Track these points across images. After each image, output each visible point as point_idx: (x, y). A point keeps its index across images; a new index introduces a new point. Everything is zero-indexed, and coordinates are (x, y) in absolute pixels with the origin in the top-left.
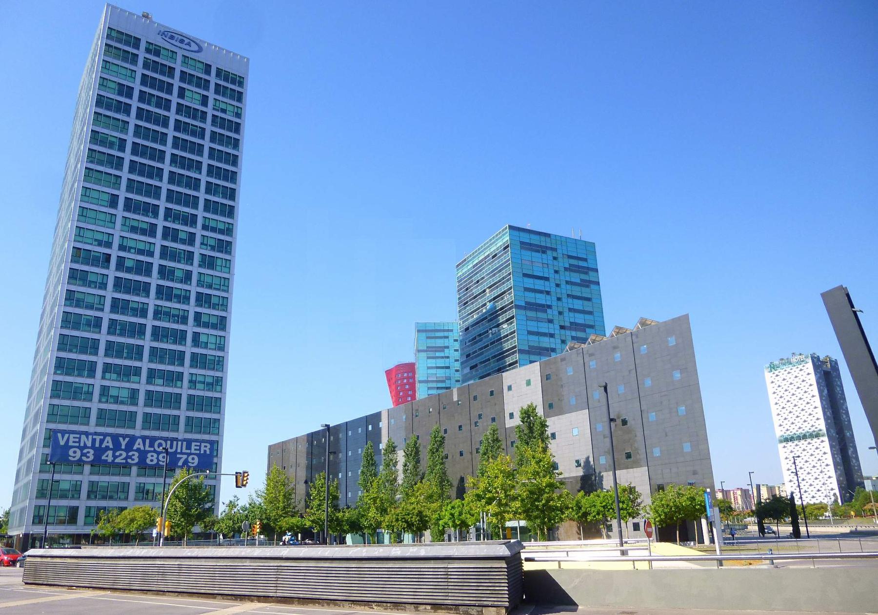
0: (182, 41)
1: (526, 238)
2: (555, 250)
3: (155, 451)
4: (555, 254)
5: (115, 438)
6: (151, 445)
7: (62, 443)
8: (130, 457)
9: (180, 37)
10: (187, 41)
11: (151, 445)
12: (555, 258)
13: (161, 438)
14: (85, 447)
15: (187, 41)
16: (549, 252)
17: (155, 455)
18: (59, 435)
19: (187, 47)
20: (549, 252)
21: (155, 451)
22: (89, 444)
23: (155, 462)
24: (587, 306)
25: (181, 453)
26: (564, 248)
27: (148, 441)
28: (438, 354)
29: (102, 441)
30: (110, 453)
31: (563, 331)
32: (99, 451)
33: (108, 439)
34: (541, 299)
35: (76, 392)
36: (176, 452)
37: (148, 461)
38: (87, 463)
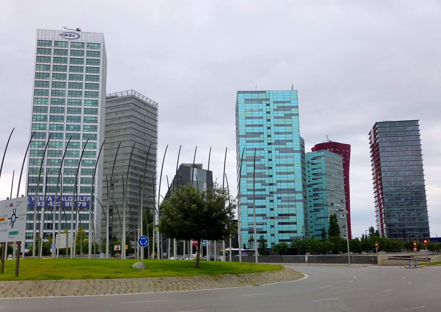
0: (70, 36)
1: (248, 96)
2: (268, 100)
3: (68, 201)
4: (268, 102)
5: (52, 197)
6: (67, 199)
7: (33, 200)
8: (59, 204)
9: (69, 34)
10: (72, 34)
11: (67, 199)
12: (268, 105)
13: (71, 196)
14: (42, 201)
15: (72, 34)
16: (264, 102)
17: (69, 203)
18: (32, 197)
19: (73, 38)
20: (264, 102)
21: (68, 201)
22: (43, 200)
23: (69, 205)
24: (288, 129)
25: (79, 201)
26: (275, 97)
27: (65, 197)
28: (255, 139)
29: (48, 198)
30: (51, 203)
31: (270, 146)
32: (47, 202)
33: (50, 197)
34: (256, 130)
35: (42, 93)
36: (77, 201)
37: (66, 205)
38: (43, 207)
